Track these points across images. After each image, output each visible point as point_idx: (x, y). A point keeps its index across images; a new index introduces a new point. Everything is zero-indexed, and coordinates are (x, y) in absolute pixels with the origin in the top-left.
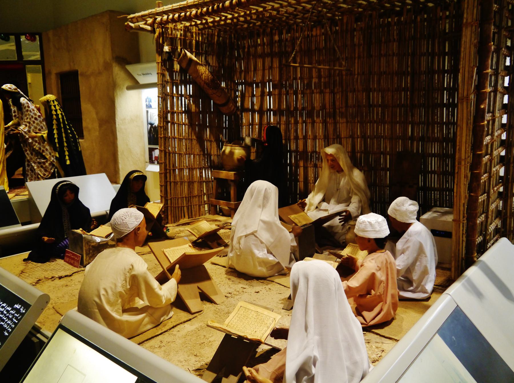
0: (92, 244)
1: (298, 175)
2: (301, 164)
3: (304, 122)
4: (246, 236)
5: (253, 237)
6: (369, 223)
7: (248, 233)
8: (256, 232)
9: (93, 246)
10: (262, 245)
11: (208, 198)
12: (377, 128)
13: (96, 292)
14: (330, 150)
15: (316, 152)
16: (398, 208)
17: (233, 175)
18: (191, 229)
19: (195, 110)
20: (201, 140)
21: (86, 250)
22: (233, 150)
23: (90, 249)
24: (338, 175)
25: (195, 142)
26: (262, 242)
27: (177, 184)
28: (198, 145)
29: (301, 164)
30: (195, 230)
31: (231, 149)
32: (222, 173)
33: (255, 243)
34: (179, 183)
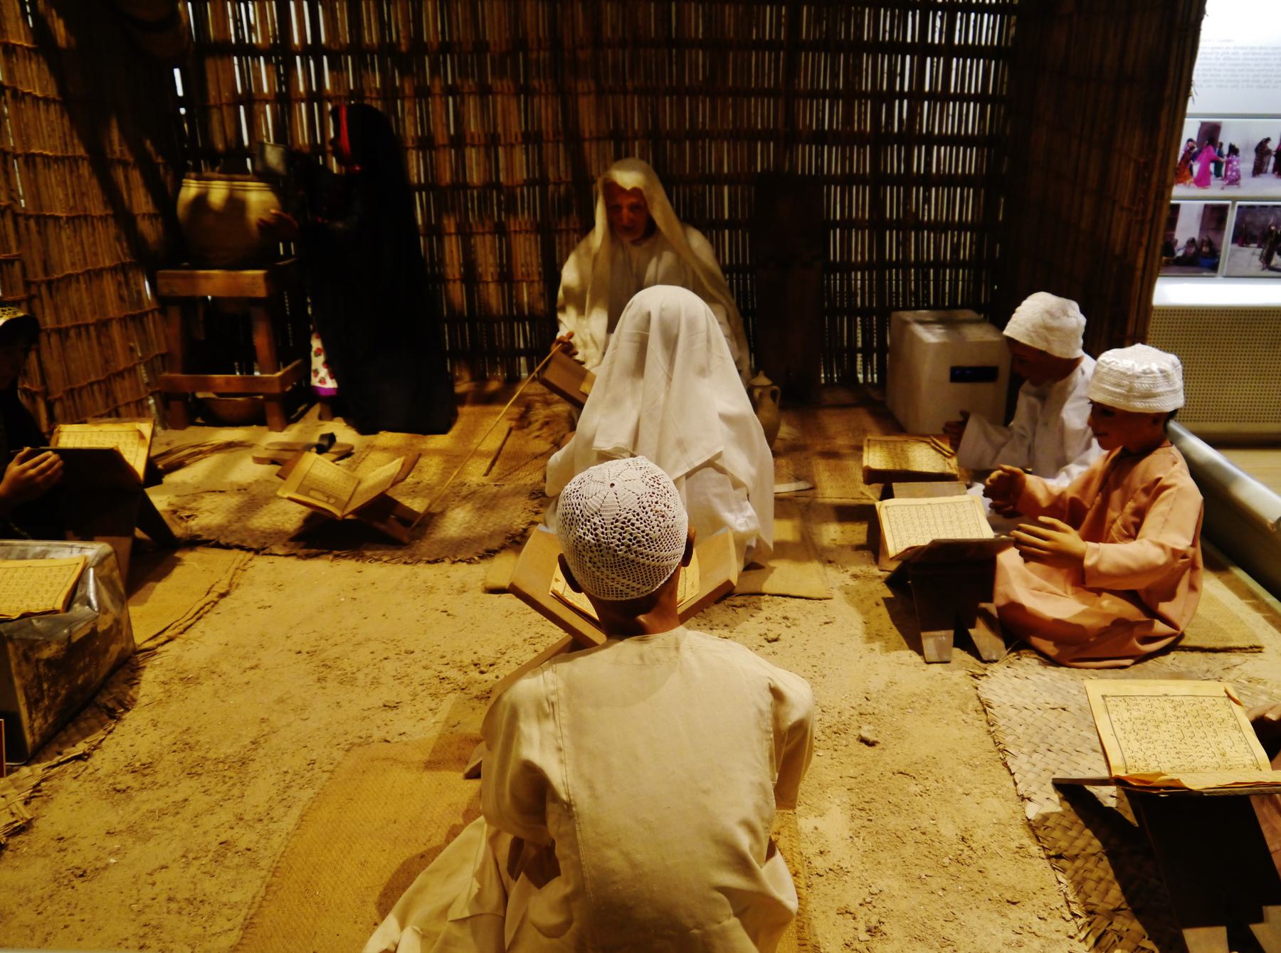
0: (46, 653)
1: (441, 262)
2: (450, 224)
3: (450, 91)
4: (688, 475)
5: (711, 473)
6: (1162, 372)
7: (697, 464)
8: (719, 455)
9: (49, 662)
10: (737, 492)
11: (151, 371)
12: (694, 111)
13: (714, 852)
14: (628, 178)
15: (497, 186)
16: (1055, 323)
17: (261, 282)
18: (297, 492)
19: (68, 42)
20: (102, 165)
21: (25, 688)
22: (240, 194)
23: (39, 678)
24: (636, 252)
25: (85, 170)
26: (737, 485)
27: (67, 336)
28: (95, 181)
29: (450, 224)
30: (312, 493)
31: (232, 190)
32: (207, 277)
33: (719, 490)
34: (72, 333)
